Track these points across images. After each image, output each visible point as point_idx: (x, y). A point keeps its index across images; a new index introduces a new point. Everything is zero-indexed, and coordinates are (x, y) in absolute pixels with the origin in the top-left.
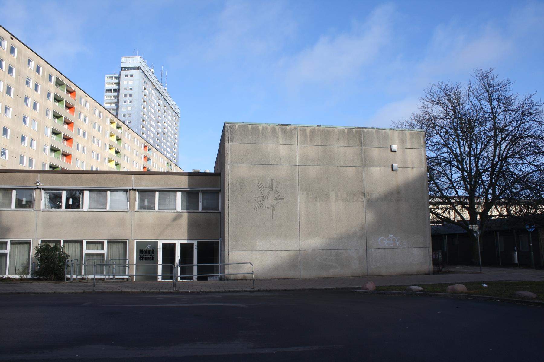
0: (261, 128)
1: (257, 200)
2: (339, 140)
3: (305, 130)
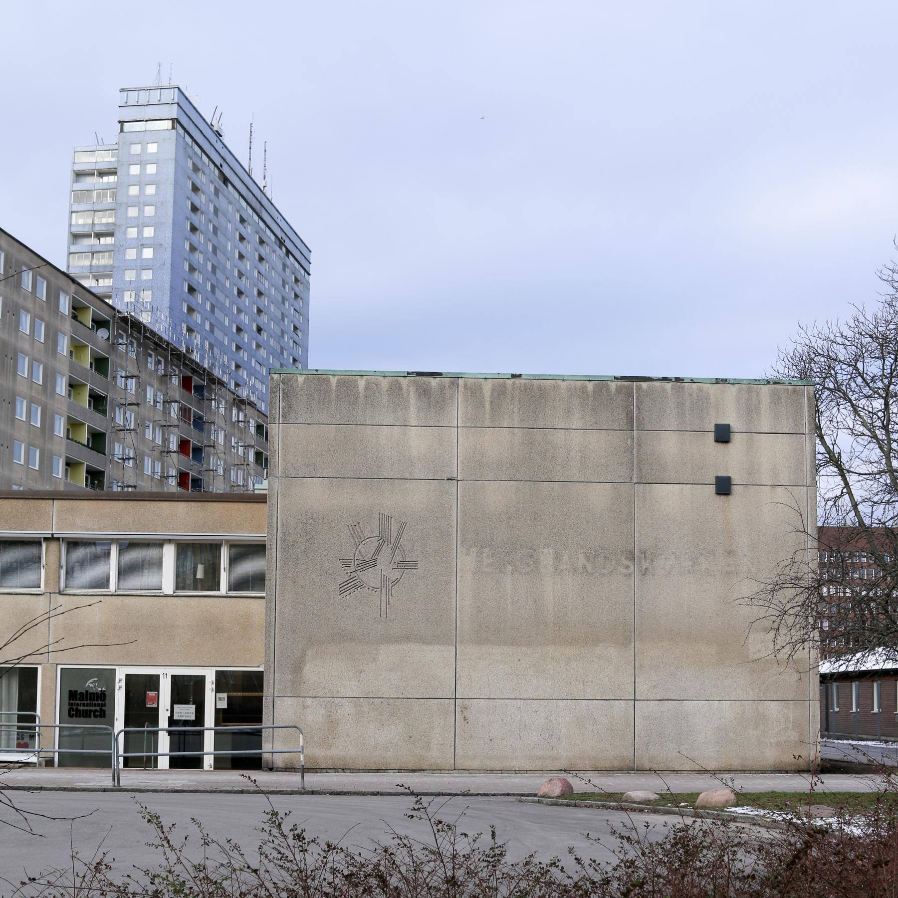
0: (362, 383)
1: (348, 570)
2: (568, 411)
3: (480, 387)
